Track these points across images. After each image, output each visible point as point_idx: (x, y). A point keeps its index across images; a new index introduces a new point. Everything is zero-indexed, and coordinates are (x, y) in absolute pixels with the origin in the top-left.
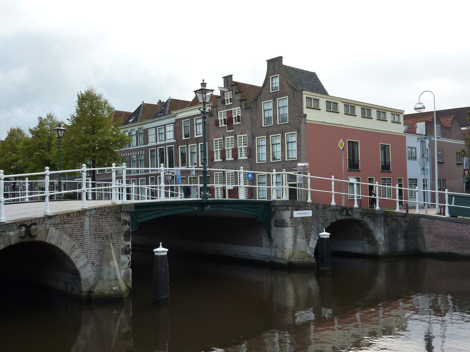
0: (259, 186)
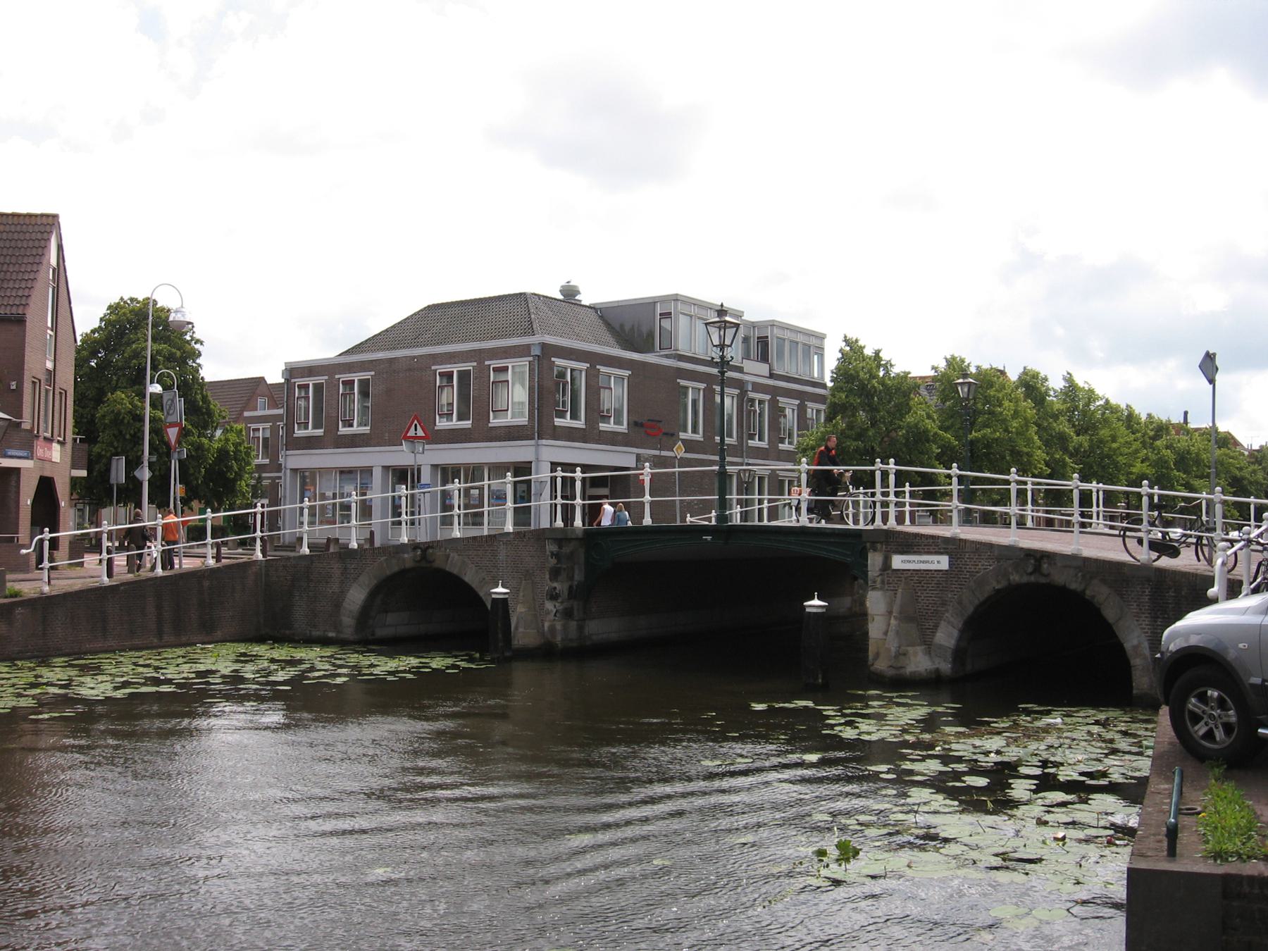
0: (760, 497)
